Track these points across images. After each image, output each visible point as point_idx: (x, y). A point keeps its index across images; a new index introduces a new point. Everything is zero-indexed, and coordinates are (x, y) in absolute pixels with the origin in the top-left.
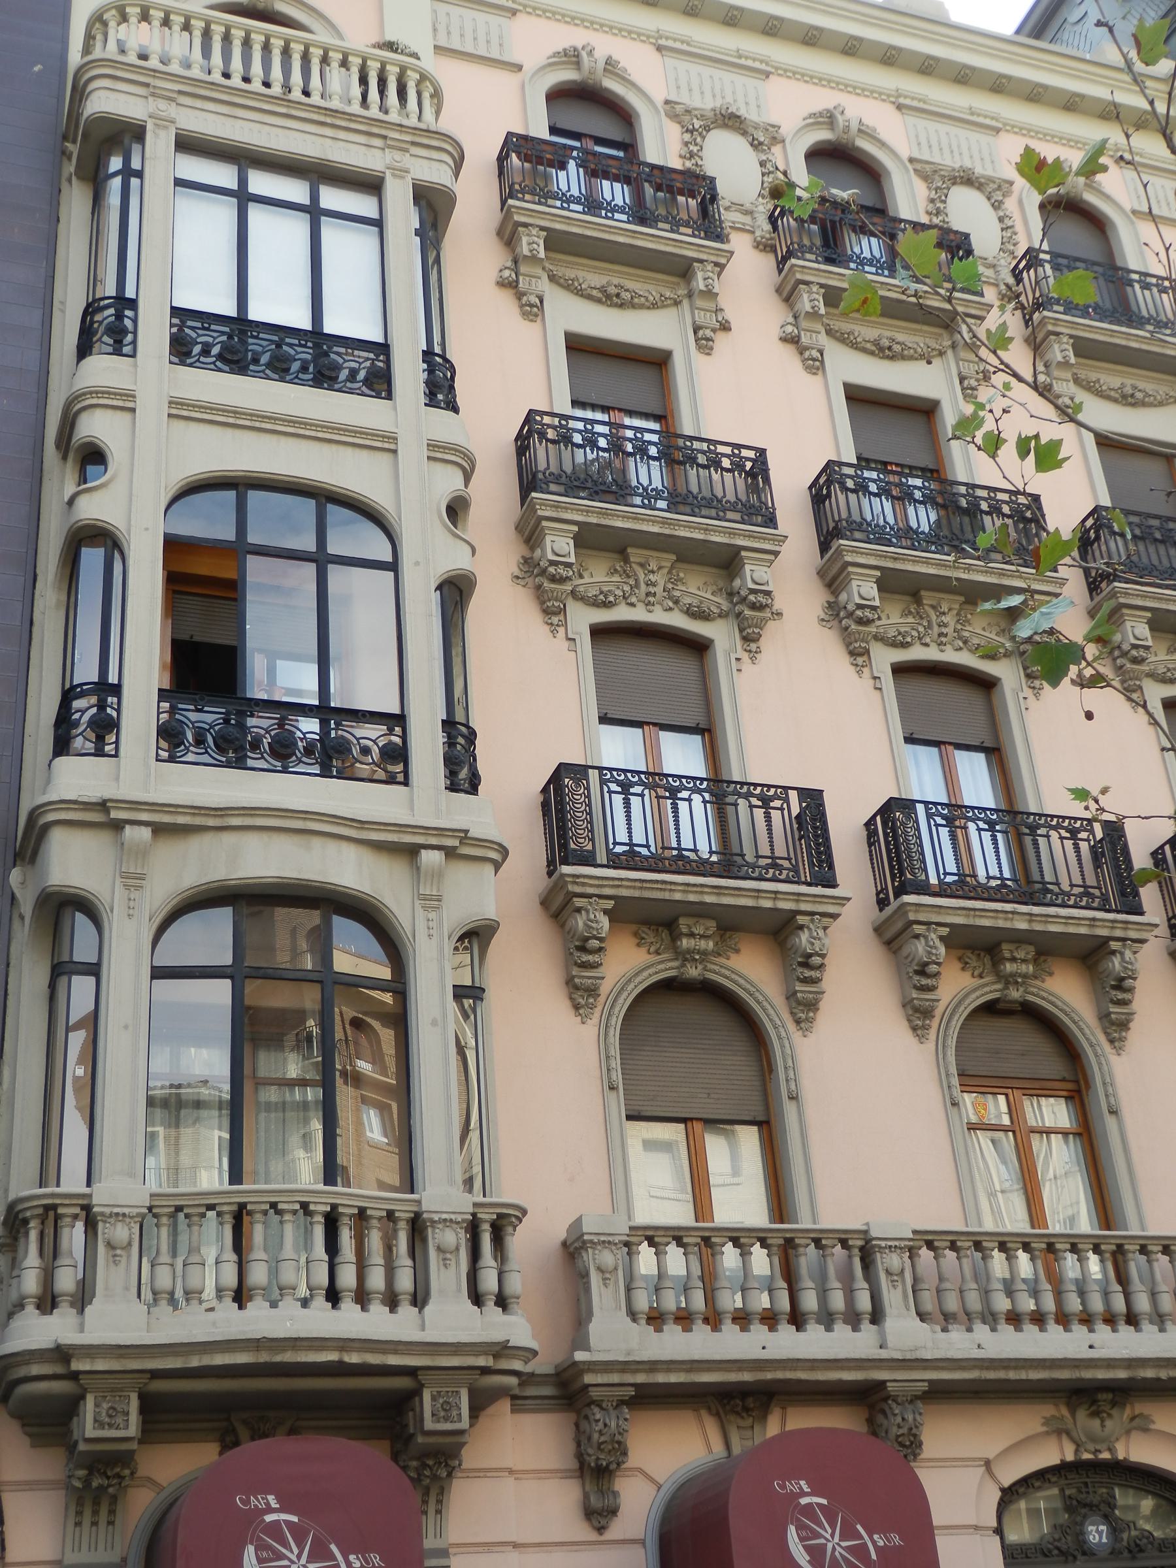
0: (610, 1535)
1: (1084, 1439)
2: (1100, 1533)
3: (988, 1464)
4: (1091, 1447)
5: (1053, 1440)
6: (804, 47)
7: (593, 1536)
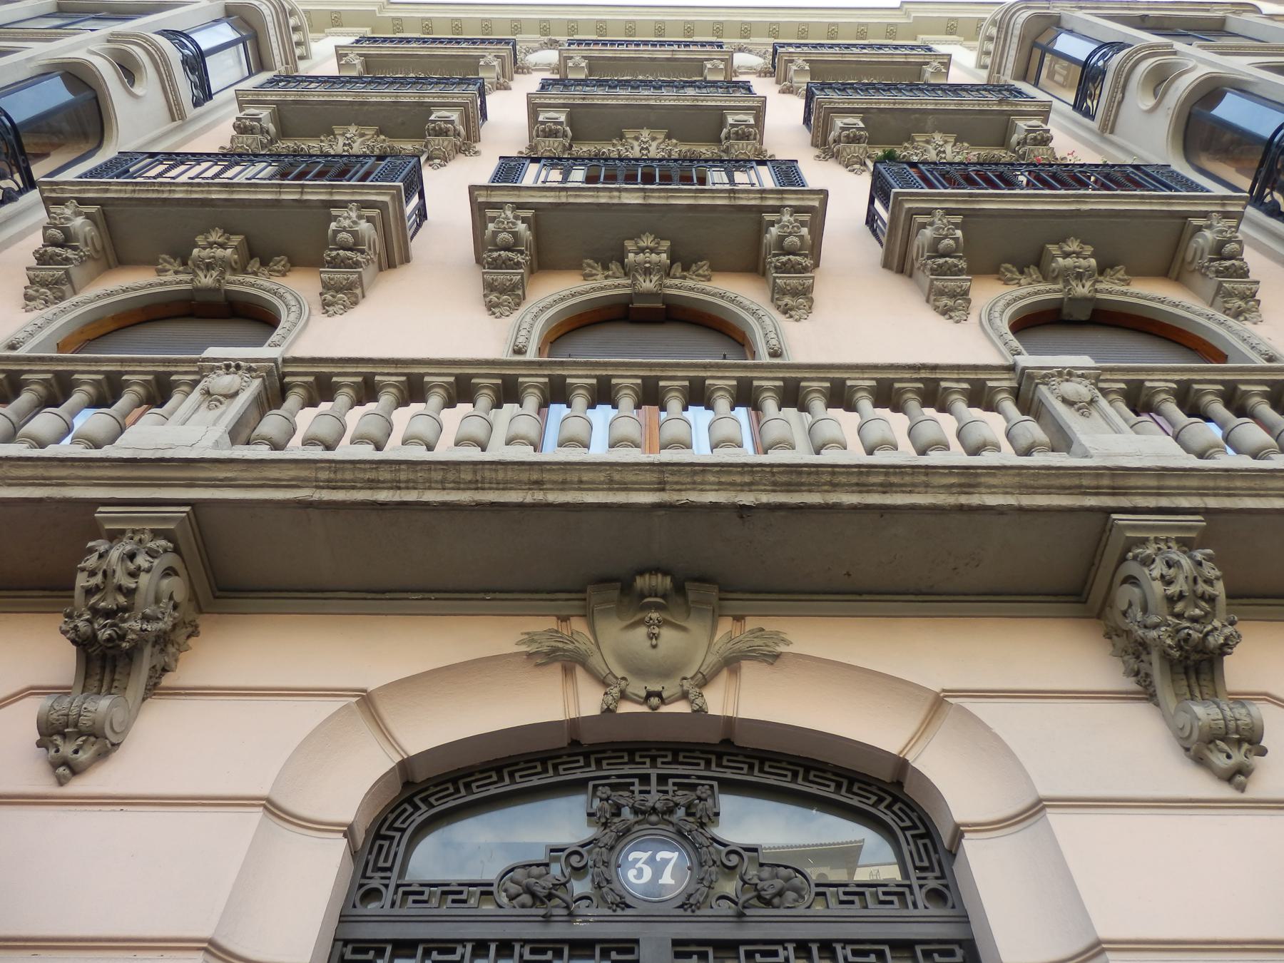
2: (658, 868)
3: (366, 700)
4: (638, 687)
5: (554, 675)
7: (45, 785)
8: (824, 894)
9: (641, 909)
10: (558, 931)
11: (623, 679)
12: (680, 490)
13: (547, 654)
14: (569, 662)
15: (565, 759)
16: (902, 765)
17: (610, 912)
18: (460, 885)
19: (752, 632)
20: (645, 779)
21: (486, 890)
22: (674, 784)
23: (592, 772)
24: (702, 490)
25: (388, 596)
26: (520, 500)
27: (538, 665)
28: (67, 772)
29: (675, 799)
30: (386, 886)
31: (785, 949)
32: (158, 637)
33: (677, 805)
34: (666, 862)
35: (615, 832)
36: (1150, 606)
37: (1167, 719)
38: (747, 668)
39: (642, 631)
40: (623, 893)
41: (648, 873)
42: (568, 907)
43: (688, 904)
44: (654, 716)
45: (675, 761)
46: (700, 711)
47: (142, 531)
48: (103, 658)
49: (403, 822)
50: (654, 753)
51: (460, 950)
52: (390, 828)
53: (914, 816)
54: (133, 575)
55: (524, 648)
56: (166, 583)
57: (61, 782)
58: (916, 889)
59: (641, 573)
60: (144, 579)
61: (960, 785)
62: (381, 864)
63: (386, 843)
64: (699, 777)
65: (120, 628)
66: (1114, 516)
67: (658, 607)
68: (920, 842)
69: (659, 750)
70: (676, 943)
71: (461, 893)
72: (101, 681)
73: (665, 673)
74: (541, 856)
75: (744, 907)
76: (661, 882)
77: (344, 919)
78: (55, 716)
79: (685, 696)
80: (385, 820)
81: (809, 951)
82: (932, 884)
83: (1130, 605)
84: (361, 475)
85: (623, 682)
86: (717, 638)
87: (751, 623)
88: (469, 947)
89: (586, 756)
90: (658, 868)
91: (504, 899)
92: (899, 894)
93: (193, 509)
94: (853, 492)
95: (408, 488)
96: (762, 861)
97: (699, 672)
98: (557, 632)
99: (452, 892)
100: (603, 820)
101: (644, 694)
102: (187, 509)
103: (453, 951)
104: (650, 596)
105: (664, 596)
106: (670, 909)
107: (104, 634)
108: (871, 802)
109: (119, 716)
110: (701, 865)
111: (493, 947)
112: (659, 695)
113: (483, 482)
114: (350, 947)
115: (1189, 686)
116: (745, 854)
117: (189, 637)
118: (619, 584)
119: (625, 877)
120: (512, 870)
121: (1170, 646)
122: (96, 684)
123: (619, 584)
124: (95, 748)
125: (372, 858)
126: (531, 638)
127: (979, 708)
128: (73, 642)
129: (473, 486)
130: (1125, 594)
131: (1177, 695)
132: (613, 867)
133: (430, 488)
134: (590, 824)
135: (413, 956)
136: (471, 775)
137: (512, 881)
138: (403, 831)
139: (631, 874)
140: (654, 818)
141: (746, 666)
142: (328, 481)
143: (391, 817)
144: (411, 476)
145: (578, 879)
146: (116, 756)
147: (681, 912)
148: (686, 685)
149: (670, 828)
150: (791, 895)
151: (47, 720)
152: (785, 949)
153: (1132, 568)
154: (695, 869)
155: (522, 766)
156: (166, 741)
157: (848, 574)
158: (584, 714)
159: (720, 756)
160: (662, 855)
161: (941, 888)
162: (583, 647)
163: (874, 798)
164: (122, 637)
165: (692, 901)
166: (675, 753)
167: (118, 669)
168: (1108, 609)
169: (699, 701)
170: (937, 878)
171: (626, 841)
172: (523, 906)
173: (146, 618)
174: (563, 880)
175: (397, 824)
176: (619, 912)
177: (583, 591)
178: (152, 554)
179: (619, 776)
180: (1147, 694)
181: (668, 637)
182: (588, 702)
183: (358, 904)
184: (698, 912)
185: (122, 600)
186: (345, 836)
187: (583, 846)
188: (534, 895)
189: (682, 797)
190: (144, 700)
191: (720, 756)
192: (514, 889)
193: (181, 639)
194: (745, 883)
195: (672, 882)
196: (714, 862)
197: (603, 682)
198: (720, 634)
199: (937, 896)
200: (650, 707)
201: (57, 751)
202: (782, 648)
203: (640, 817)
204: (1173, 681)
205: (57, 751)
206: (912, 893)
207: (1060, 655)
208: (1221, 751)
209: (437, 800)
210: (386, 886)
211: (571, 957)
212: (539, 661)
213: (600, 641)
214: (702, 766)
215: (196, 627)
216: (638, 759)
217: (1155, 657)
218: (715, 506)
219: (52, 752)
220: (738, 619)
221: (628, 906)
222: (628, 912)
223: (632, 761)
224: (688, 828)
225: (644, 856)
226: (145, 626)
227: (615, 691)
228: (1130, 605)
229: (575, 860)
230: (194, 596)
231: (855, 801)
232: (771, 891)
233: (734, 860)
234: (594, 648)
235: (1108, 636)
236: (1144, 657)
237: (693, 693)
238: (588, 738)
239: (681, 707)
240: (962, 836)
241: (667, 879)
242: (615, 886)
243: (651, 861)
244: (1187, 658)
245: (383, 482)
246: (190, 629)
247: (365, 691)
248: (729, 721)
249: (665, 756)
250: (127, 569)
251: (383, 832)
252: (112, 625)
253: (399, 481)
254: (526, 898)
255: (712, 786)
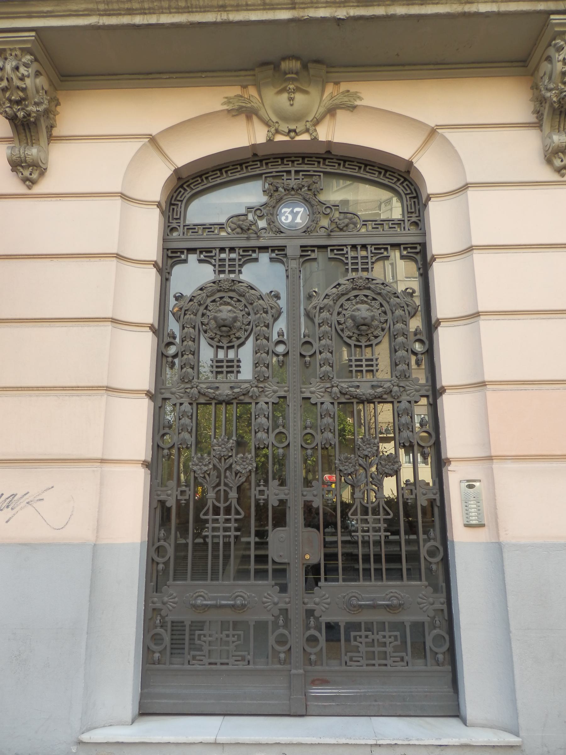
0: (37, 189)
1: (275, 119)
2: (295, 215)
3: (153, 140)
4: (284, 127)
5: (242, 121)
6: (152, 510)
7: (21, 189)
8: (366, 225)
9: (288, 233)
10: (253, 243)
11: (277, 122)
12: (304, 8)
13: (237, 110)
14: (248, 113)
15: (251, 163)
16: (410, 164)
17: (274, 235)
18: (210, 225)
19: (343, 93)
20: (289, 172)
21: (221, 226)
22: (303, 175)
23: (264, 170)
24: (316, 8)
25: (150, 76)
26: (214, 20)
27: (233, 116)
28: (30, 184)
29: (303, 183)
30: (179, 226)
31: (347, 248)
32: (44, 113)
33: (303, 186)
34: (298, 213)
35: (276, 199)
36: (553, 77)
37: (543, 139)
38: (340, 114)
39: (285, 96)
40: (280, 227)
41: (290, 218)
42: (256, 233)
43: (307, 231)
44: (292, 142)
45: (303, 163)
46: (315, 139)
47: (15, 49)
48: (23, 125)
49: (181, 197)
50: (293, 159)
51: (214, 251)
52: (175, 200)
53: (412, 188)
54: (22, 79)
55: (225, 107)
56: (38, 81)
57: (29, 188)
58: (406, 221)
59: (284, 59)
60: (28, 81)
61: (434, 175)
62: (175, 217)
63: (175, 207)
64: (314, 171)
65: (27, 111)
66: (552, 17)
67: (293, 80)
68: (413, 200)
69: (295, 157)
70: (301, 247)
71: (211, 228)
72: (26, 136)
73: (298, 118)
74: (243, 211)
75: (331, 232)
76: (296, 221)
77: (164, 240)
78: (14, 158)
79: (307, 131)
80: (172, 197)
81: (357, 248)
82: (414, 219)
83: (545, 74)
84: (122, 6)
85: (277, 125)
86: (324, 97)
87: (344, 87)
88: (218, 250)
89: (261, 161)
90: (295, 215)
91: (229, 230)
92: (399, 223)
93: (37, 33)
94: (404, 5)
95: (150, 13)
96: (341, 211)
97: (315, 117)
98: (241, 96)
99: (208, 228)
100: (270, 194)
101: (287, 131)
102: (33, 34)
103: (211, 252)
104: (289, 73)
105: (297, 73)
106: (299, 233)
107: (21, 114)
108: (393, 182)
109: (42, 156)
110: (313, 214)
111: (227, 250)
112: (295, 131)
113: (192, 8)
114: (170, 251)
115: (559, 122)
116: (333, 208)
117: (56, 106)
118: (272, 66)
119: (281, 220)
120: (232, 217)
121: (555, 102)
122: (24, 138)
123: (272, 66)
124: (38, 172)
125: (171, 214)
126: (229, 101)
127: (450, 135)
128: (6, 118)
129: (186, 10)
130: (545, 67)
131: (551, 126)
132: (275, 216)
133: (163, 13)
134: (264, 195)
135: (196, 253)
136: (208, 173)
137: (232, 222)
138: (182, 201)
139: (283, 218)
140: (293, 193)
141: (339, 112)
142: (105, 10)
143: (175, 195)
144: (151, 5)
145: (261, 220)
146: (48, 173)
147: (304, 234)
148: (308, 125)
149: (300, 197)
150: (351, 226)
151: (12, 160)
152: (347, 248)
153: (551, 51)
154: (311, 216)
155: (231, 168)
156: (68, 164)
157: (398, 55)
158: (258, 142)
159: (325, 159)
160: (296, 210)
161: (417, 221)
162: (255, 105)
163: (395, 180)
164: (29, 115)
165: (309, 230)
166: (303, 158)
167: (32, 130)
168: (536, 72)
169: (314, 134)
170: (417, 217)
171: (280, 203)
172: (238, 233)
173: (36, 104)
174: (254, 222)
175: (178, 198)
176: (278, 235)
177: (253, 69)
178: (26, 65)
179: (277, 172)
180: (538, 125)
181: (299, 97)
182: (259, 135)
183: (169, 234)
184: (311, 234)
185: (21, 94)
186: (158, 206)
187: (261, 206)
188: (242, 229)
189: (307, 181)
190: (48, 144)
191: (325, 159)
192: (233, 226)
193: (53, 108)
194: (332, 222)
195: (301, 221)
196: (319, 213)
197: (267, 124)
198: (326, 94)
199: (416, 224)
200: (290, 138)
201: (22, 174)
202: (358, 103)
203: (287, 192)
204: (552, 119)
205: (22, 174)
206: (404, 223)
207: (502, 102)
208: (560, 158)
209: (194, 186)
210: (179, 226)
211: (259, 252)
212: (234, 114)
213: (264, 101)
214: (316, 165)
215: (58, 100)
216: (285, 162)
217: (547, 106)
218: (323, 19)
219: (20, 175)
220: (337, 83)
221: (282, 232)
222: (282, 235)
223: (283, 163)
224: (308, 197)
225: (288, 210)
226: (38, 109)
227: (273, 130)
228: (545, 74)
229: (258, 212)
230: (51, 83)
231: (386, 182)
232: (343, 225)
233: (328, 210)
234: (261, 105)
235: (532, 88)
236: (543, 104)
237: (312, 129)
238: (261, 153)
239: (305, 137)
240: (430, 199)
241: (298, 220)
242: (276, 224)
243: (292, 212)
244: (562, 107)
245: (136, 9)
246: (55, 102)
247: (151, 135)
248: (329, 143)
249: (299, 161)
250: (17, 76)
251: (173, 202)
252: (23, 109)
253: (145, 9)
254: (238, 230)
255: (320, 176)
